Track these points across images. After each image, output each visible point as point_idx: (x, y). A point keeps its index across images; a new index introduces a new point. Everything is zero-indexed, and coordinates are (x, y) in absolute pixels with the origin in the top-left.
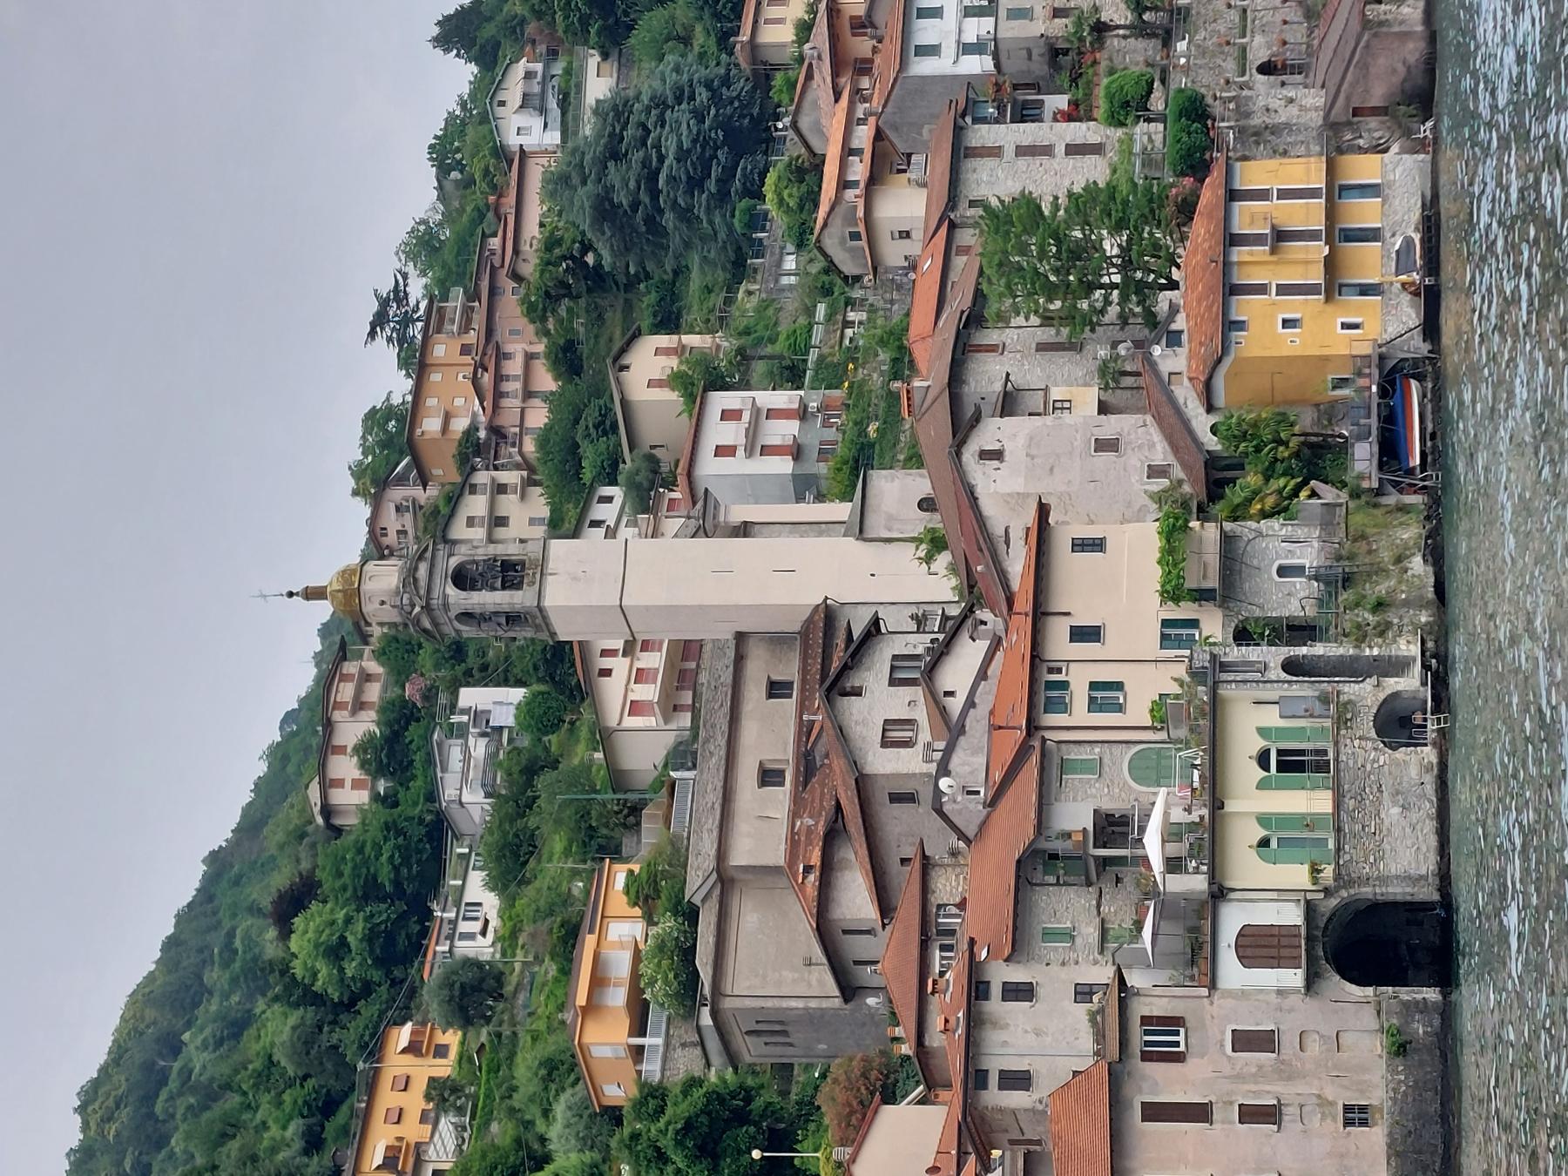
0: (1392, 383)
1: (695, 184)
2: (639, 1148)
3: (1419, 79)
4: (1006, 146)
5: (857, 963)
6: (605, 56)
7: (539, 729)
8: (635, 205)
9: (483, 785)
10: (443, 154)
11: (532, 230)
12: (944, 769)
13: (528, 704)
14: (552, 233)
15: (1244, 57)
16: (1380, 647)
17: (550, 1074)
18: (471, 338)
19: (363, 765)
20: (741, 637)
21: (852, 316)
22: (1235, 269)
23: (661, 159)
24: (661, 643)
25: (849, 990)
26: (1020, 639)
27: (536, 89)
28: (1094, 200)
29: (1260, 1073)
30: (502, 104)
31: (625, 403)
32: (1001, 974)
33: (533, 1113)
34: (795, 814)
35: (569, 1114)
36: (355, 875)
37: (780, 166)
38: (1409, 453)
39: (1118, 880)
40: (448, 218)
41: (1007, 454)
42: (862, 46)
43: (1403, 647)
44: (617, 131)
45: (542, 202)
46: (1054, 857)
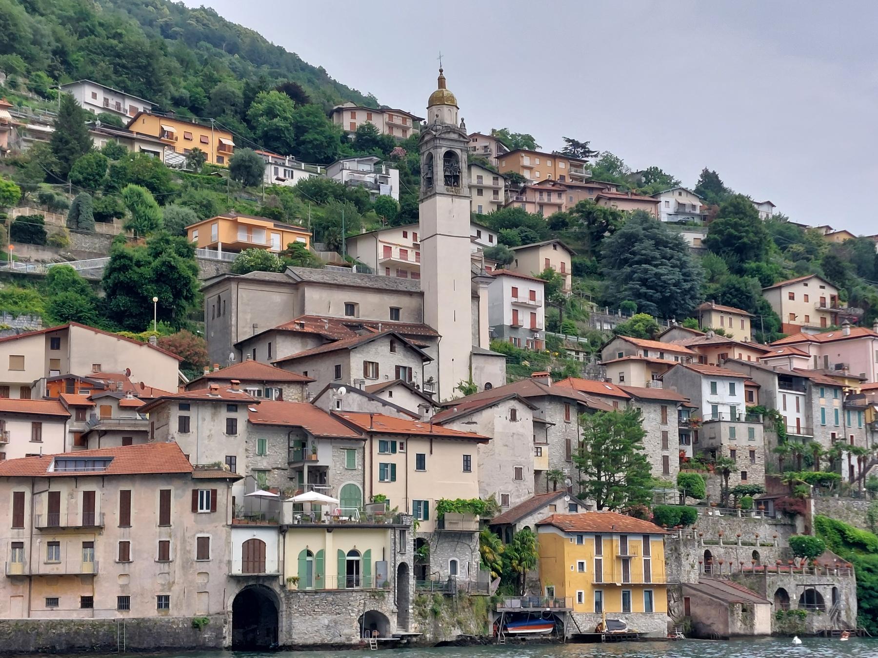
0: (551, 619)
1: (644, 282)
2: (162, 244)
3: (704, 631)
5: (254, 350)
6: (704, 242)
7: (378, 206)
8: (634, 253)
9: (351, 180)
10: (653, 174)
11: (621, 206)
12: (350, 390)
13: (391, 201)
14: (619, 216)
15: (713, 544)
16: (413, 613)
17: (204, 206)
18: (568, 181)
19: (362, 127)
20: (421, 294)
21: (581, 355)
22: (609, 538)
23: (656, 266)
24: (419, 262)
25: (240, 347)
26: (418, 428)
27: (687, 210)
28: (643, 468)
29: (185, 552)
30: (680, 194)
31: (539, 246)
32: (241, 418)
33: (184, 197)
34: (331, 320)
35: (184, 214)
36: (308, 122)
37: (653, 321)
38: (514, 627)
39: (291, 479)
40: (623, 176)
41: (514, 423)
42: (713, 359)
43: (413, 625)
44: (669, 245)
45: (634, 211)
46: (304, 445)
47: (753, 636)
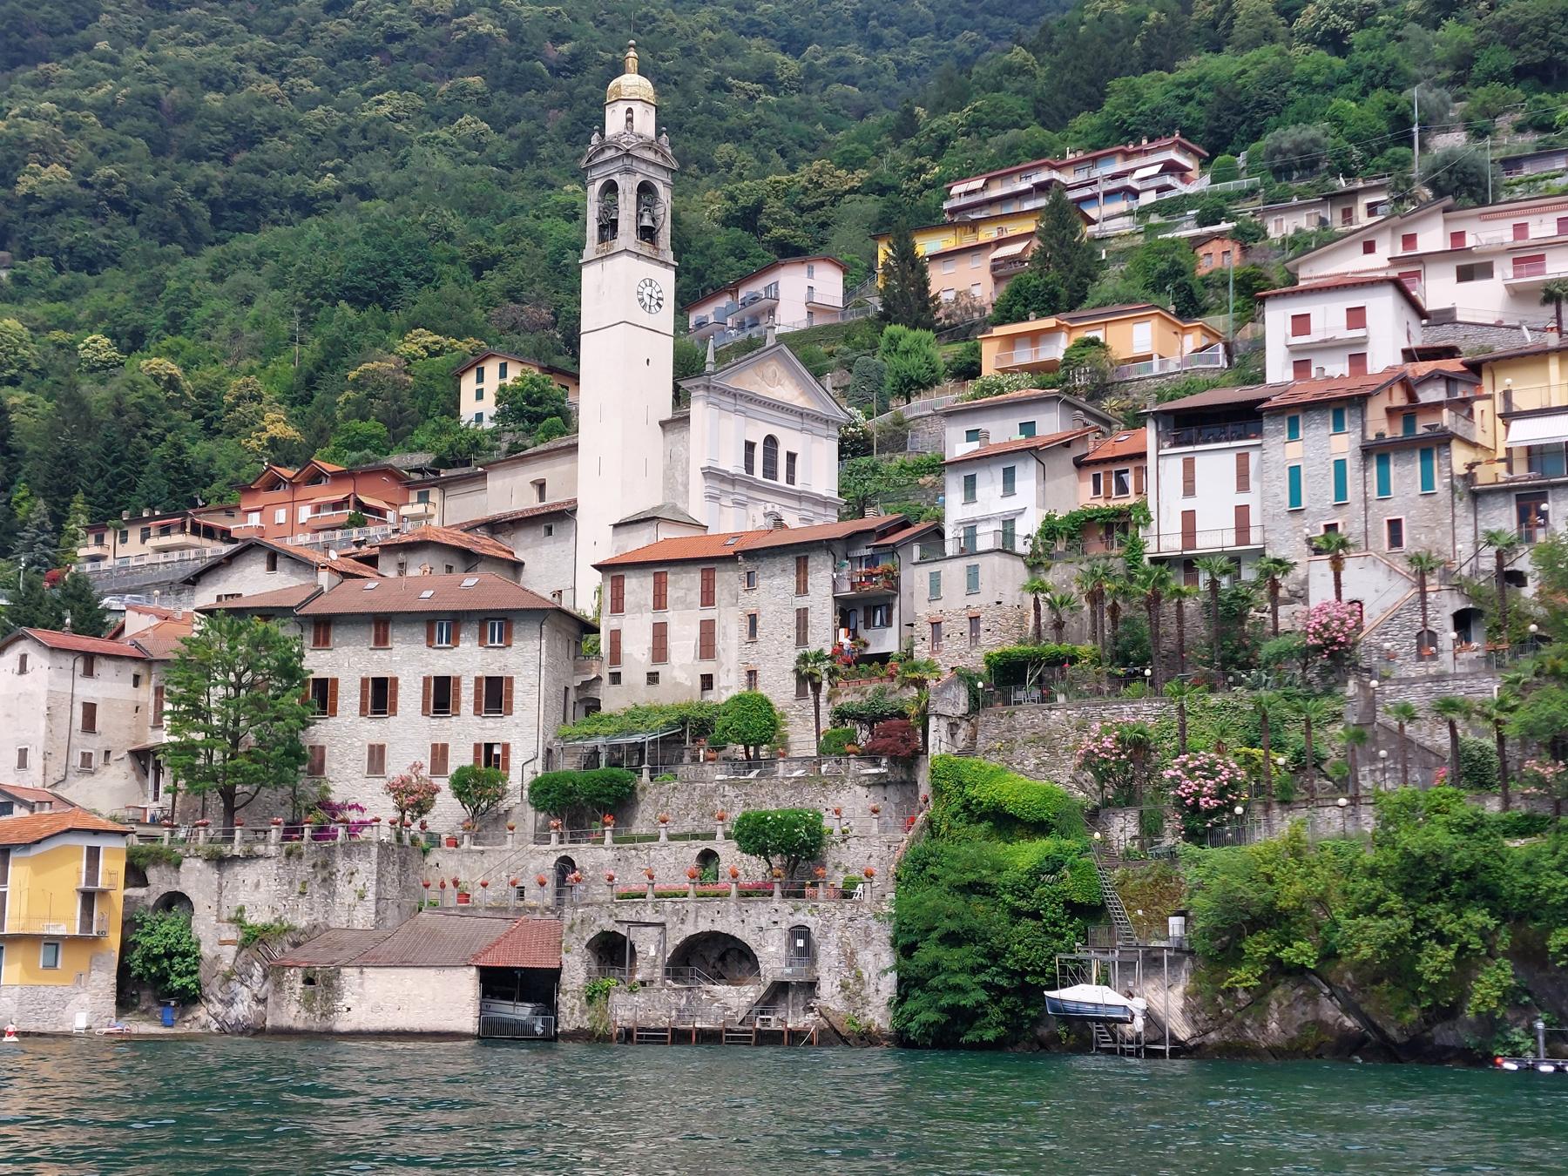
47: (330, 1035)
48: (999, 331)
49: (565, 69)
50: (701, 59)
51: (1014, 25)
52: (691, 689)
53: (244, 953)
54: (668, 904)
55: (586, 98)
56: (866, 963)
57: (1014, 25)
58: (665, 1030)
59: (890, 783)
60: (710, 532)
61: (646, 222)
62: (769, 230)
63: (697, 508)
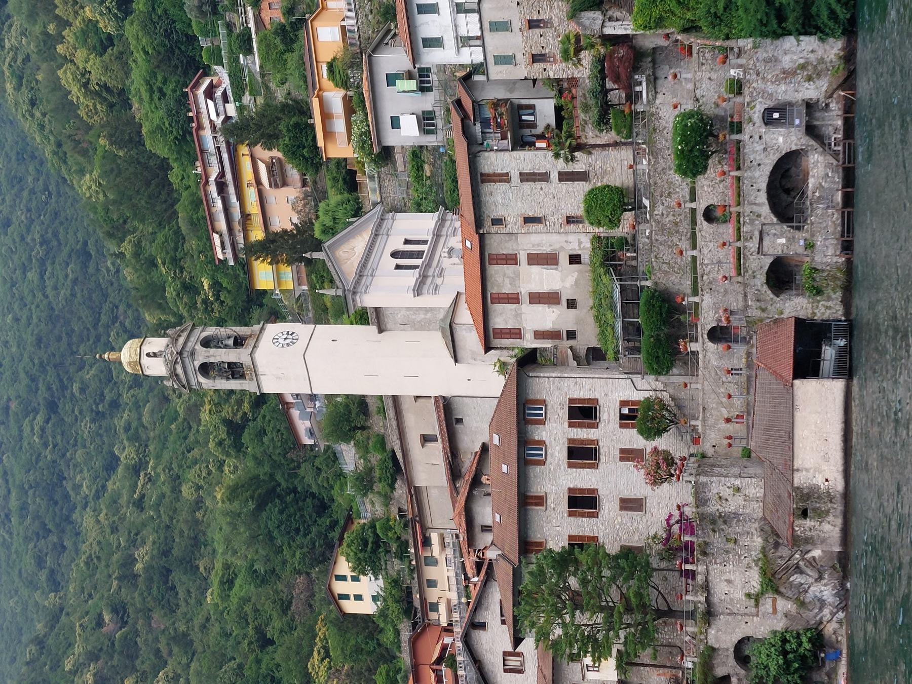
4: (512, 172)
47: (847, 495)
48: (320, 143)
49: (122, 618)
50: (120, 519)
51: (106, 307)
52: (580, 272)
53: (782, 590)
54: (745, 229)
55: (144, 599)
56: (792, 61)
57: (106, 307)
58: (843, 213)
59: (654, 74)
60: (463, 290)
61: (231, 342)
62: (245, 414)
63: (443, 301)
